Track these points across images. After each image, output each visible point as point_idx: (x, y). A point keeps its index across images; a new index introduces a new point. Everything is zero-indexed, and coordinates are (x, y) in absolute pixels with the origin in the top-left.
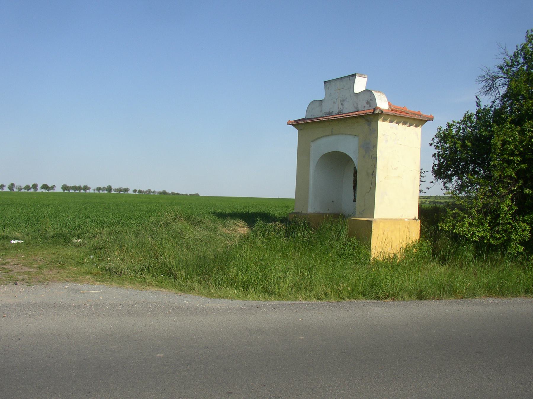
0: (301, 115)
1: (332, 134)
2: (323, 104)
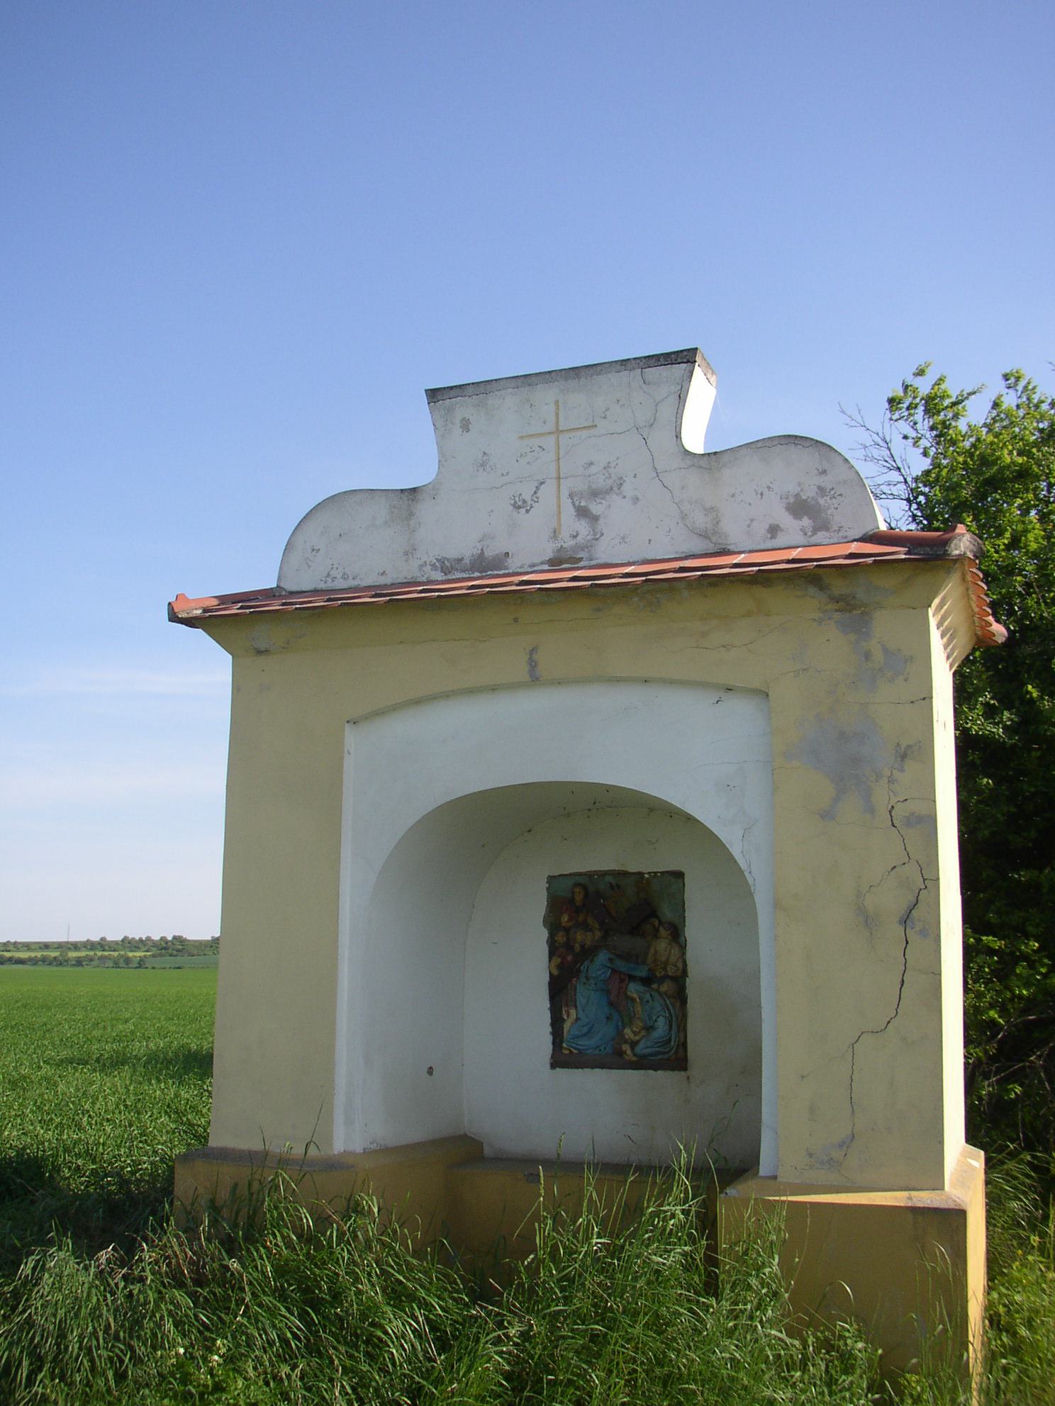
0: (256, 572)
1: (535, 679)
2: (426, 511)
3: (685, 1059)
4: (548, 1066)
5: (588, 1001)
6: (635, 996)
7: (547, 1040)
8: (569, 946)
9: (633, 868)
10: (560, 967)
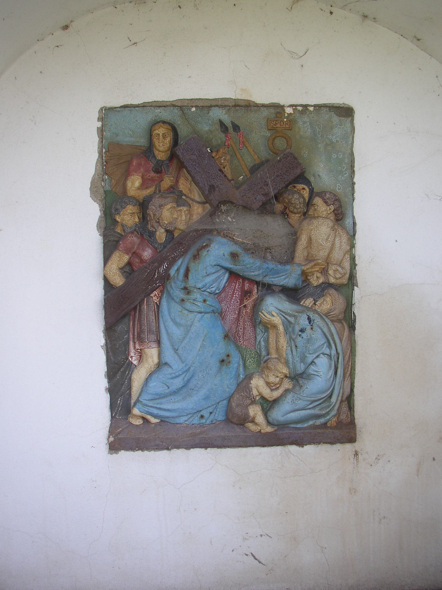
3: (352, 424)
4: (104, 448)
5: (187, 331)
6: (277, 320)
7: (102, 401)
8: (144, 230)
9: (261, 97)
10: (128, 270)
